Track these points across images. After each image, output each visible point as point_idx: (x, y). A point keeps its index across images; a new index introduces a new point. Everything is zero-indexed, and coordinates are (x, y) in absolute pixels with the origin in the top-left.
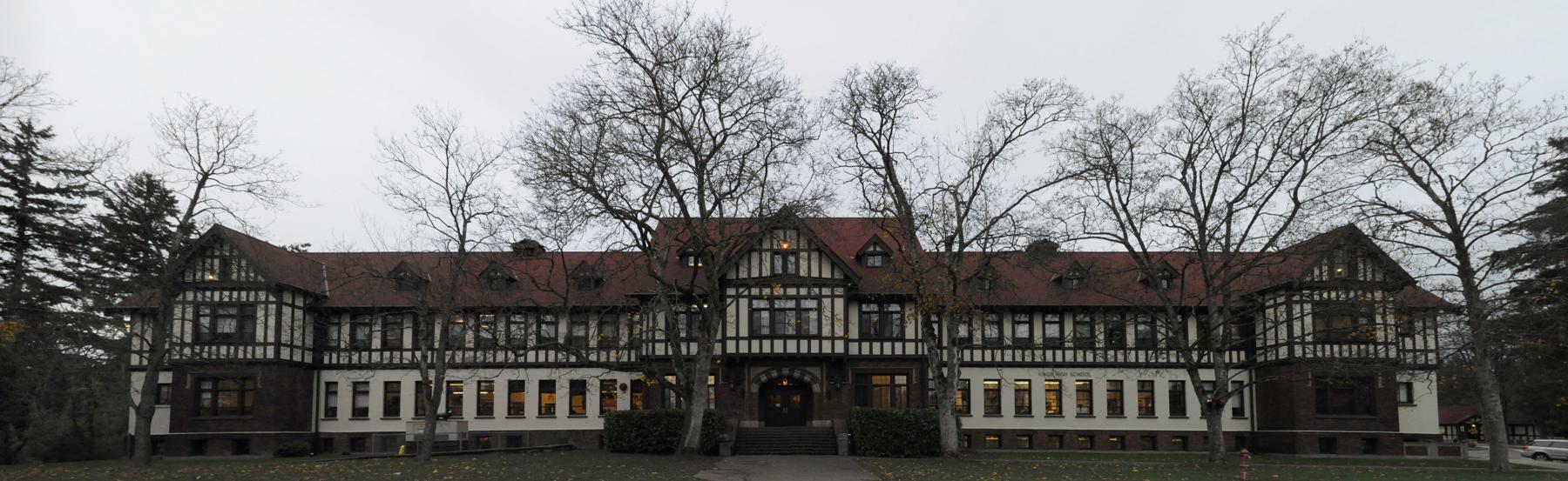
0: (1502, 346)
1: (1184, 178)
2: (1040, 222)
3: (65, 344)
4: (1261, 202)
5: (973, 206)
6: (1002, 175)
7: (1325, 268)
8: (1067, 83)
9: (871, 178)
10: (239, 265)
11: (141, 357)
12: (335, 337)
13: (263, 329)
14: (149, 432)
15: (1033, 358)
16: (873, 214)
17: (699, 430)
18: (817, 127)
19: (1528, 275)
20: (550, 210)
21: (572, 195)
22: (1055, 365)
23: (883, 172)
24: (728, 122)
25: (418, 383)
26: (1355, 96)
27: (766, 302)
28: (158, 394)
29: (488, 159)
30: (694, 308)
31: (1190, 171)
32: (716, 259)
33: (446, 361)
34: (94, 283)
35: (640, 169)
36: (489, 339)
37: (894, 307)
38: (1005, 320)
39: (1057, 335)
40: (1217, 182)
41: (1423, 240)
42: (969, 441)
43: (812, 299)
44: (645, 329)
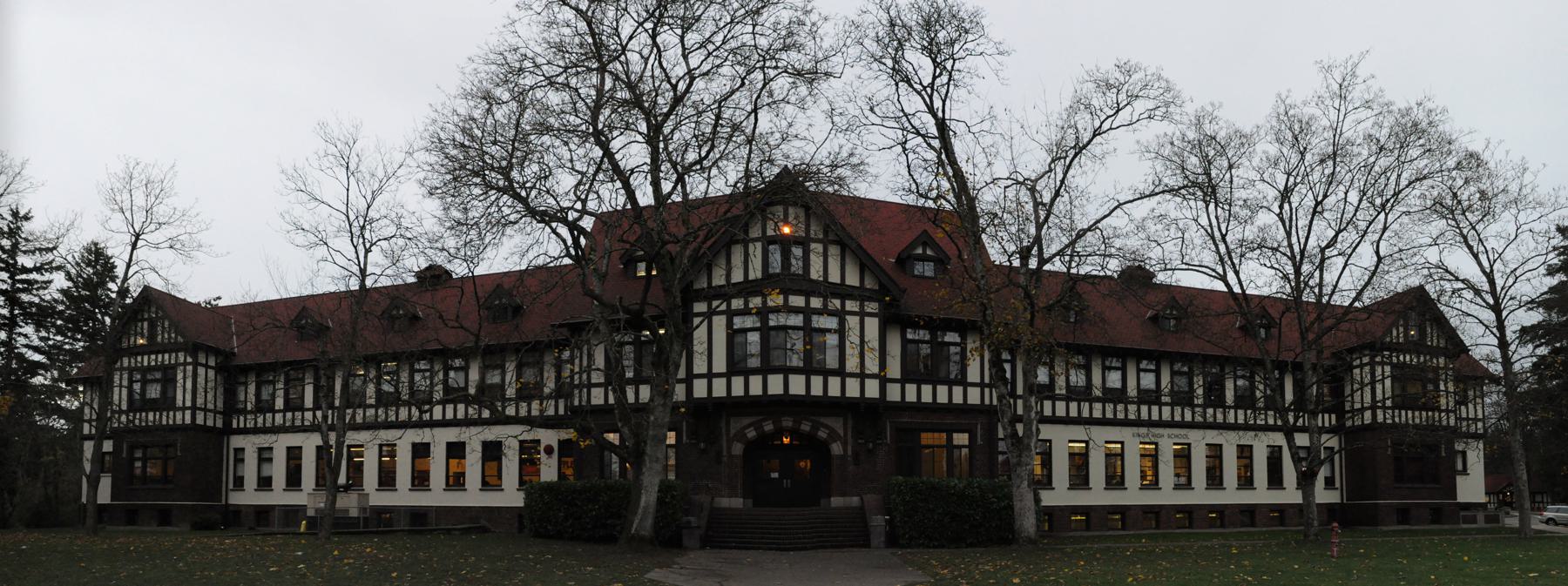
0: (1527, 418)
1: (1281, 213)
2: (1133, 243)
3: (40, 415)
4: (1349, 251)
5: (1055, 210)
6: (1091, 175)
7: (1401, 329)
8: (1164, 74)
9: (919, 149)
10: (163, 327)
11: (91, 425)
12: (242, 398)
13: (182, 396)
14: (96, 500)
15: (1126, 415)
16: (921, 202)
17: (652, 510)
18: (838, 59)
19: (1543, 351)
20: (459, 223)
21: (485, 199)
22: (1151, 424)
23: (936, 143)
24: (694, 61)
25: (318, 448)
26: (1424, 153)
27: (755, 318)
28: (103, 462)
29: (390, 171)
30: (647, 336)
31: (1286, 206)
32: (677, 261)
33: (347, 421)
34: (58, 355)
35: (570, 150)
36: (391, 393)
37: (952, 337)
38: (1093, 363)
39: (1153, 386)
40: (1311, 222)
41: (1474, 309)
42: (1050, 521)
43: (829, 315)
44: (577, 369)
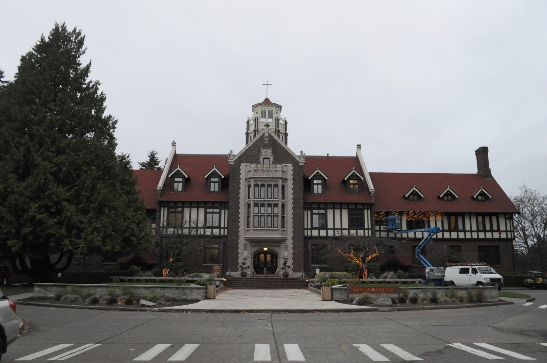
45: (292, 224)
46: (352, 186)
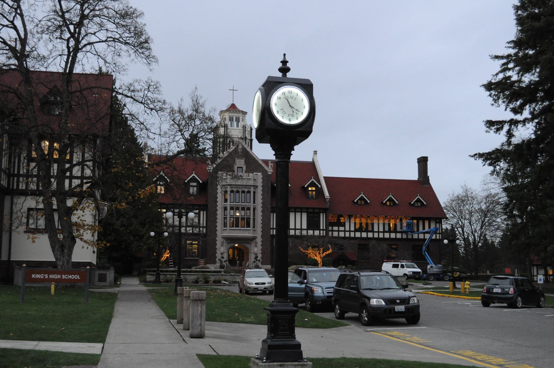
37: (415, 221)
45: (261, 225)
46: (310, 193)
